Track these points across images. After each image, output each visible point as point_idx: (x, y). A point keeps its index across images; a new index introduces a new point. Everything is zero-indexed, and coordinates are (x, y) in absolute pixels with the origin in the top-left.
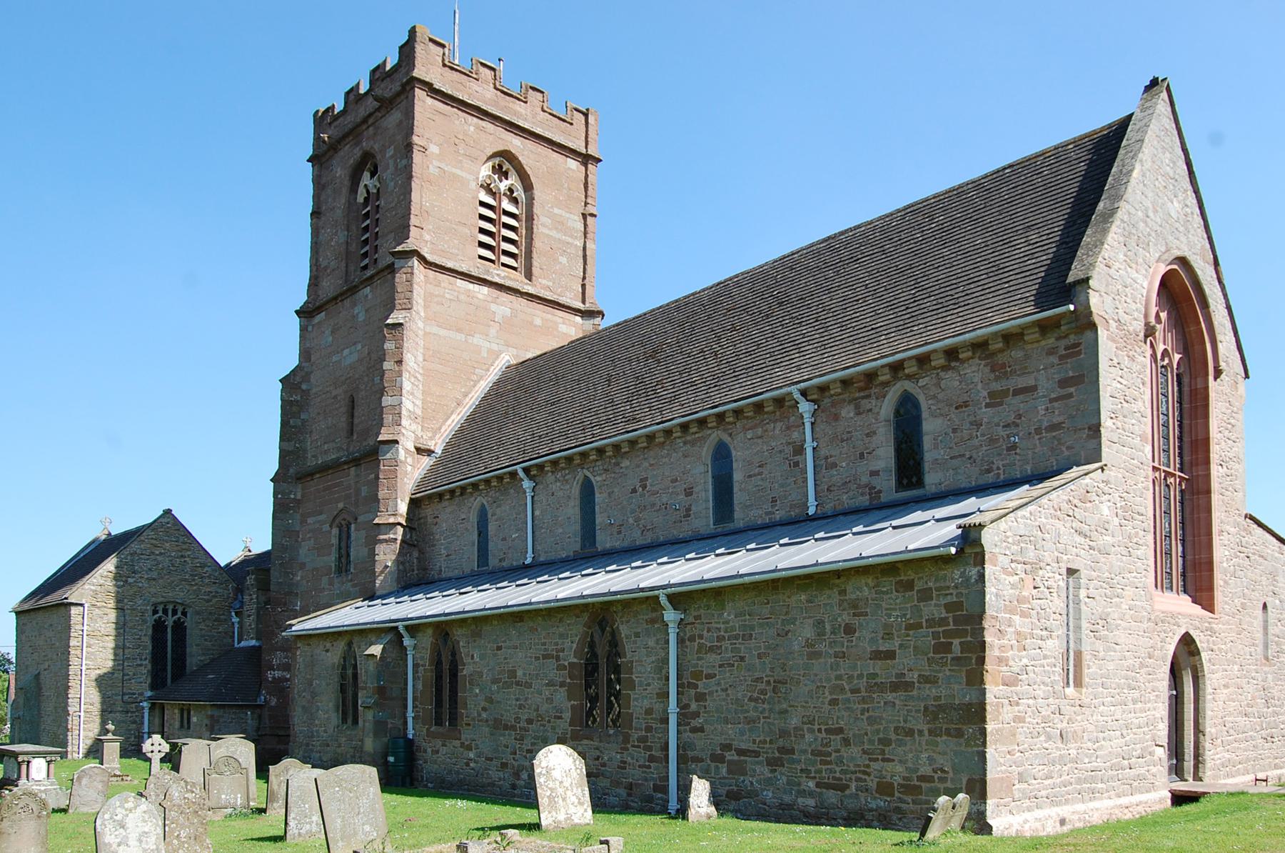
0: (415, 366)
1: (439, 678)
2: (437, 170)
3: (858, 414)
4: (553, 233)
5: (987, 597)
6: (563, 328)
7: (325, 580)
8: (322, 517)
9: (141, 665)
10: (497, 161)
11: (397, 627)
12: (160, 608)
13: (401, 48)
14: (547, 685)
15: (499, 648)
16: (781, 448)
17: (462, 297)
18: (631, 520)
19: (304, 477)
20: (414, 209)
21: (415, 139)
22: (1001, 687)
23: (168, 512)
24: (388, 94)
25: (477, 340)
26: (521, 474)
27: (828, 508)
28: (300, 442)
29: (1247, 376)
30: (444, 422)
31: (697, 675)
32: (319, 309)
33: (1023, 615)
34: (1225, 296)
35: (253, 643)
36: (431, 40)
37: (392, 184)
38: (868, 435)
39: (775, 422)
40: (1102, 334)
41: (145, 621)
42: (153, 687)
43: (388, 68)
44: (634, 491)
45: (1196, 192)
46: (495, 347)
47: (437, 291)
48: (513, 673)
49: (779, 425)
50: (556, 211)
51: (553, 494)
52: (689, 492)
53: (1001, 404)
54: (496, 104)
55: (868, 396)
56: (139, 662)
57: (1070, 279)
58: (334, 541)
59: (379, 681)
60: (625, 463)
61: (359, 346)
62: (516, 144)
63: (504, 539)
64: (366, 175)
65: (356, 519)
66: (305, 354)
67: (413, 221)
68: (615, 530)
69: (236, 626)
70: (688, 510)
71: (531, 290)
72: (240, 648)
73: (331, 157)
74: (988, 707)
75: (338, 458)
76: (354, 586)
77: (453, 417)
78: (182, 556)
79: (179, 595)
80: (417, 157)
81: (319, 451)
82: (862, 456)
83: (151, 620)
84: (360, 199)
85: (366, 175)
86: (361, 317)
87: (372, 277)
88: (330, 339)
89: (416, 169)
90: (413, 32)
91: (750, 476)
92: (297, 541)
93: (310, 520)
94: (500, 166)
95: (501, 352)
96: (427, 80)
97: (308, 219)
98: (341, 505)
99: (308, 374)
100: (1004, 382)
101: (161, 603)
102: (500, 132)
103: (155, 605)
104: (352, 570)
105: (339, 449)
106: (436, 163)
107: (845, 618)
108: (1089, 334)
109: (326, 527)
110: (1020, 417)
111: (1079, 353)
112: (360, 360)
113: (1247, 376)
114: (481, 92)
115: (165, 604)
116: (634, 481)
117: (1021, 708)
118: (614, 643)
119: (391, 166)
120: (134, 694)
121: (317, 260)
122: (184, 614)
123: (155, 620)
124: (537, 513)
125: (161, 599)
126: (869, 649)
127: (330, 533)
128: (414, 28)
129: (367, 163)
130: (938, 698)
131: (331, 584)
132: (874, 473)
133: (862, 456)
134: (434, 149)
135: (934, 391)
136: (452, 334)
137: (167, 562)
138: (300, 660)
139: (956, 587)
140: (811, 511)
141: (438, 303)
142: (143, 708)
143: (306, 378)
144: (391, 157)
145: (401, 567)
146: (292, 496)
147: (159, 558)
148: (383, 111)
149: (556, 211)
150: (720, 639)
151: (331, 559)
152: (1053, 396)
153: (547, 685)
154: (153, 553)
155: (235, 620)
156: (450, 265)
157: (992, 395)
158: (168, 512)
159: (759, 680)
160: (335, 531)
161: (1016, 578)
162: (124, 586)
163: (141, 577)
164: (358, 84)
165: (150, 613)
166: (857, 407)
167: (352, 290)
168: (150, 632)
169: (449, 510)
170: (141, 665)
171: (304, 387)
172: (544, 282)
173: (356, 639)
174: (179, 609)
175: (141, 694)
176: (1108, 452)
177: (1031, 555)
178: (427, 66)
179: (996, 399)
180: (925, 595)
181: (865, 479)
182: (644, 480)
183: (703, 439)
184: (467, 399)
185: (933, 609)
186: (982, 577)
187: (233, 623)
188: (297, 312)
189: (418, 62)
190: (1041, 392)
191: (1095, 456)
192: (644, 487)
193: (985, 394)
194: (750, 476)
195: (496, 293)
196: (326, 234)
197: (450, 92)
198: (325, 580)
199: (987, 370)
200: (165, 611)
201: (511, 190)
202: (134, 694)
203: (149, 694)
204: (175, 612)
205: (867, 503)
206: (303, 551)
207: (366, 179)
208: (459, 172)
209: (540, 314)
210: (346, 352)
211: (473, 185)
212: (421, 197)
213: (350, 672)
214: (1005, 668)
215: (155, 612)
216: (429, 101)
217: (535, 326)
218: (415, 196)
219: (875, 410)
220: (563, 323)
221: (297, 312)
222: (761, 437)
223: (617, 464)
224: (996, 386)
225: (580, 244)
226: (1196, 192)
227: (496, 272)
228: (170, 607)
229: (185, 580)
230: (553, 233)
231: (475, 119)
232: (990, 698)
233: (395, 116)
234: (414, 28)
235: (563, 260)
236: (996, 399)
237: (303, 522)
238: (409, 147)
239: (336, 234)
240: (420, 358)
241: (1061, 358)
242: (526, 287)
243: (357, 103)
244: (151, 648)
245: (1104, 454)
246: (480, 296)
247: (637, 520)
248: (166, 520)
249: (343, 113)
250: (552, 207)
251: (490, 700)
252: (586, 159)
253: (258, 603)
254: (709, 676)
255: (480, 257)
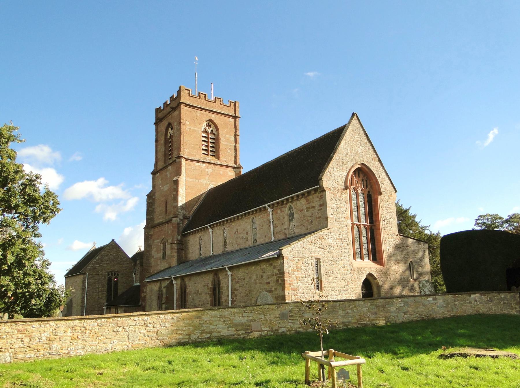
0: (183, 192)
1: (182, 293)
2: (189, 129)
3: (281, 212)
4: (226, 143)
5: (285, 268)
6: (230, 174)
7: (159, 261)
8: (159, 240)
9: (104, 294)
10: (208, 122)
11: (171, 278)
12: (110, 273)
13: (177, 91)
14: (205, 294)
15: (195, 283)
16: (266, 221)
17: (197, 168)
18: (235, 242)
19: (154, 227)
20: (182, 143)
21: (182, 121)
22: (291, 291)
23: (113, 240)
24: (174, 106)
25: (202, 181)
26: (209, 227)
27: (276, 239)
28: (153, 215)
29: (396, 191)
30: (192, 209)
31: (235, 290)
32: (157, 172)
33: (298, 271)
34: (385, 170)
35: (138, 284)
36: (186, 89)
37: (176, 134)
38: (283, 218)
39: (265, 213)
40: (328, 193)
41: (105, 278)
42: (107, 302)
43: (175, 97)
44: (235, 233)
45: (370, 142)
46: (208, 183)
47: (189, 167)
48: (198, 291)
49: (265, 214)
50: (226, 136)
51: (217, 233)
52: (247, 234)
53: (309, 211)
54: (206, 105)
55: (283, 207)
56: (103, 293)
57: (318, 179)
58: (162, 248)
59: (166, 295)
60: (233, 224)
61: (168, 185)
62: (213, 117)
63: (206, 247)
64: (170, 129)
65: (167, 241)
66: (154, 187)
67: (182, 146)
68: (231, 244)
69: (134, 278)
70: (247, 239)
71: (219, 162)
72: (135, 286)
73: (160, 123)
74: (286, 296)
75: (163, 221)
76: (167, 263)
77: (195, 206)
78: (117, 255)
79: (116, 269)
80: (182, 126)
81: (158, 219)
82: (283, 224)
83: (107, 278)
84: (168, 137)
85: (170, 129)
86: (169, 176)
87: (171, 163)
88: (160, 182)
89: (182, 130)
90: (180, 88)
91: (260, 229)
92: (151, 249)
93: (155, 241)
94: (209, 124)
95: (210, 184)
96: (184, 102)
97: (154, 143)
98: (163, 237)
99: (155, 193)
100: (309, 205)
101: (111, 271)
102: (207, 113)
103: (109, 272)
104: (166, 258)
105: (163, 218)
106: (188, 127)
107: (261, 273)
108: (324, 192)
109: (159, 244)
110: (312, 214)
111: (323, 197)
112: (168, 190)
113: (396, 191)
114: (202, 104)
115: (112, 272)
116: (235, 230)
117: (298, 296)
118: (219, 281)
119: (176, 128)
120: (101, 304)
121: (157, 156)
122: (118, 275)
123: (109, 278)
124: (213, 239)
125: (110, 270)
126: (265, 282)
127: (160, 245)
128: (180, 86)
129: (170, 125)
130: (277, 294)
131: (161, 262)
132: (285, 229)
133: (283, 224)
134: (188, 123)
135: (296, 206)
136: (195, 180)
137: (113, 258)
138: (148, 289)
139: (280, 265)
140: (273, 240)
141: (190, 171)
142: (104, 309)
143: (154, 194)
144: (176, 125)
145: (179, 257)
146: (150, 234)
147: (110, 256)
148: (173, 111)
149: (226, 136)
150: (239, 279)
151: (160, 255)
152: (318, 209)
153: (205, 294)
154: (108, 255)
155: (134, 276)
156: (193, 159)
157: (307, 208)
158: (113, 240)
159: (246, 290)
160: (162, 245)
161: (295, 262)
162: (99, 266)
163: (105, 263)
164: (167, 101)
165: (107, 275)
166: (281, 210)
167: (166, 167)
168: (107, 282)
169: (192, 238)
170: (104, 294)
171: (153, 197)
172: (223, 159)
173: (186, 279)
174: (116, 274)
175: (103, 304)
176: (329, 225)
177: (301, 255)
178: (185, 98)
179: (308, 209)
180: (274, 267)
181: (283, 231)
182: (237, 230)
183: (249, 218)
184: (199, 200)
185: (276, 271)
186: (283, 262)
187: (133, 277)
188: (151, 173)
189: (182, 97)
190: (316, 208)
191: (326, 226)
192: (237, 232)
193: (305, 208)
194: (260, 229)
195: (208, 165)
196: (159, 147)
197: (192, 105)
198: (159, 261)
199: (306, 201)
200: (112, 274)
201: (212, 131)
202: (101, 304)
203: (106, 304)
204: (115, 274)
205: (284, 238)
206: (153, 252)
207: (170, 131)
208: (195, 129)
209: (222, 170)
210: (165, 186)
211: (200, 132)
212: (184, 139)
213: (161, 292)
214: (292, 286)
215: (109, 275)
216: (186, 108)
217: (221, 174)
218: (182, 139)
219: (285, 211)
220: (230, 172)
221: (151, 173)
222: (262, 218)
223: (231, 225)
224: (308, 206)
225: (234, 145)
226: (370, 142)
227: (208, 158)
228: (113, 273)
229: (119, 263)
230: (226, 143)
231: (200, 111)
232: (287, 294)
233: (176, 113)
234: (180, 86)
235: (229, 151)
236: (308, 209)
237: (153, 242)
238: (180, 123)
239: (162, 148)
240: (184, 189)
241: (320, 199)
242: (217, 162)
243: (167, 107)
244: (107, 287)
245: (329, 225)
246: (203, 167)
247: (236, 242)
248: (112, 243)
249: (163, 109)
250: (225, 135)
251: (193, 299)
252: (235, 117)
253: (140, 270)
254: (237, 290)
255: (203, 154)
